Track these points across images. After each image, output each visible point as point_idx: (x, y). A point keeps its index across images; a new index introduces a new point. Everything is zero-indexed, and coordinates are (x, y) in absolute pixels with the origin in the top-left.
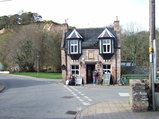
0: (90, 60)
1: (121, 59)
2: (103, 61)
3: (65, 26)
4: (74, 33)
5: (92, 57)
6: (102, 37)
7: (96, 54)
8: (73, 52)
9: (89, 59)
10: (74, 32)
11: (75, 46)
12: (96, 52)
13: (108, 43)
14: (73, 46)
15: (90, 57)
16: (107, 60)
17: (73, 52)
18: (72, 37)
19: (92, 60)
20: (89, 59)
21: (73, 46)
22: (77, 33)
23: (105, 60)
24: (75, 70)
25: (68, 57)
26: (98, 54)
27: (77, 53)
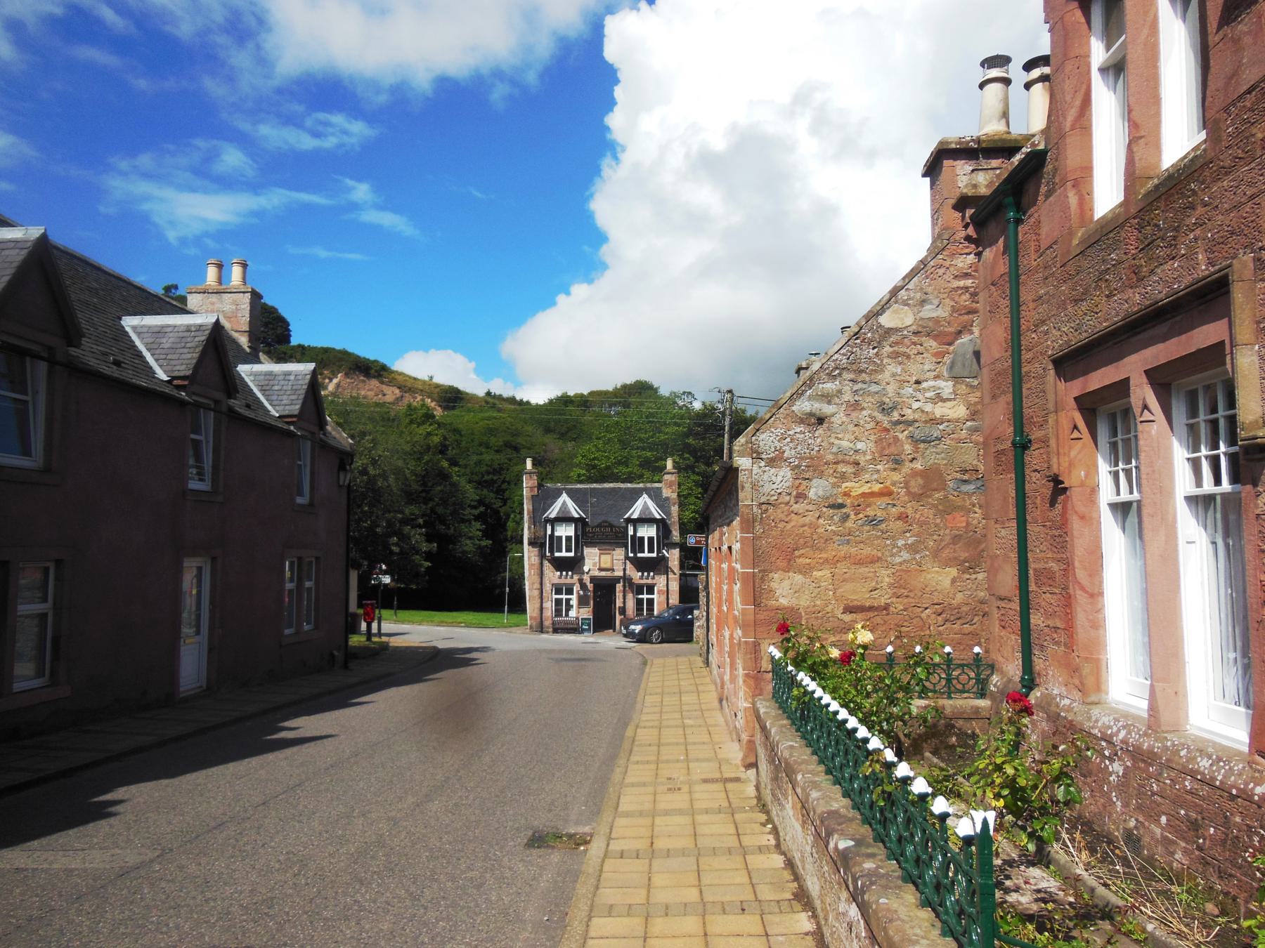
0: (603, 574)
1: (1130, 403)
2: (636, 576)
3: (530, 476)
4: (139, 334)
5: (608, 565)
6: (635, 516)
7: (618, 558)
8: (561, 551)
9: (601, 569)
10: (564, 502)
11: (644, 552)
12: (619, 553)
13: (647, 532)
14: (649, 552)
15: (603, 566)
16: (646, 574)
17: (561, 551)
18: (560, 515)
19: (608, 574)
20: (601, 569)
21: (649, 552)
22: (571, 505)
23: (640, 574)
24: (564, 597)
25: (546, 564)
26: (623, 557)
27: (654, 555)
